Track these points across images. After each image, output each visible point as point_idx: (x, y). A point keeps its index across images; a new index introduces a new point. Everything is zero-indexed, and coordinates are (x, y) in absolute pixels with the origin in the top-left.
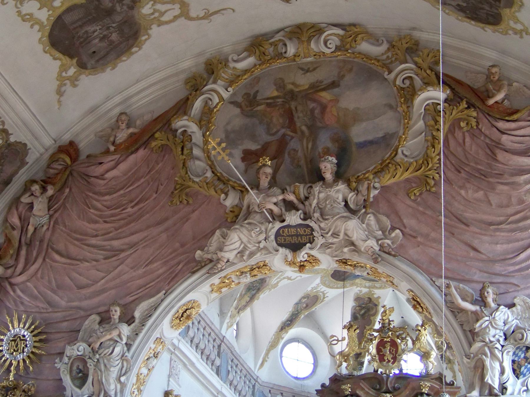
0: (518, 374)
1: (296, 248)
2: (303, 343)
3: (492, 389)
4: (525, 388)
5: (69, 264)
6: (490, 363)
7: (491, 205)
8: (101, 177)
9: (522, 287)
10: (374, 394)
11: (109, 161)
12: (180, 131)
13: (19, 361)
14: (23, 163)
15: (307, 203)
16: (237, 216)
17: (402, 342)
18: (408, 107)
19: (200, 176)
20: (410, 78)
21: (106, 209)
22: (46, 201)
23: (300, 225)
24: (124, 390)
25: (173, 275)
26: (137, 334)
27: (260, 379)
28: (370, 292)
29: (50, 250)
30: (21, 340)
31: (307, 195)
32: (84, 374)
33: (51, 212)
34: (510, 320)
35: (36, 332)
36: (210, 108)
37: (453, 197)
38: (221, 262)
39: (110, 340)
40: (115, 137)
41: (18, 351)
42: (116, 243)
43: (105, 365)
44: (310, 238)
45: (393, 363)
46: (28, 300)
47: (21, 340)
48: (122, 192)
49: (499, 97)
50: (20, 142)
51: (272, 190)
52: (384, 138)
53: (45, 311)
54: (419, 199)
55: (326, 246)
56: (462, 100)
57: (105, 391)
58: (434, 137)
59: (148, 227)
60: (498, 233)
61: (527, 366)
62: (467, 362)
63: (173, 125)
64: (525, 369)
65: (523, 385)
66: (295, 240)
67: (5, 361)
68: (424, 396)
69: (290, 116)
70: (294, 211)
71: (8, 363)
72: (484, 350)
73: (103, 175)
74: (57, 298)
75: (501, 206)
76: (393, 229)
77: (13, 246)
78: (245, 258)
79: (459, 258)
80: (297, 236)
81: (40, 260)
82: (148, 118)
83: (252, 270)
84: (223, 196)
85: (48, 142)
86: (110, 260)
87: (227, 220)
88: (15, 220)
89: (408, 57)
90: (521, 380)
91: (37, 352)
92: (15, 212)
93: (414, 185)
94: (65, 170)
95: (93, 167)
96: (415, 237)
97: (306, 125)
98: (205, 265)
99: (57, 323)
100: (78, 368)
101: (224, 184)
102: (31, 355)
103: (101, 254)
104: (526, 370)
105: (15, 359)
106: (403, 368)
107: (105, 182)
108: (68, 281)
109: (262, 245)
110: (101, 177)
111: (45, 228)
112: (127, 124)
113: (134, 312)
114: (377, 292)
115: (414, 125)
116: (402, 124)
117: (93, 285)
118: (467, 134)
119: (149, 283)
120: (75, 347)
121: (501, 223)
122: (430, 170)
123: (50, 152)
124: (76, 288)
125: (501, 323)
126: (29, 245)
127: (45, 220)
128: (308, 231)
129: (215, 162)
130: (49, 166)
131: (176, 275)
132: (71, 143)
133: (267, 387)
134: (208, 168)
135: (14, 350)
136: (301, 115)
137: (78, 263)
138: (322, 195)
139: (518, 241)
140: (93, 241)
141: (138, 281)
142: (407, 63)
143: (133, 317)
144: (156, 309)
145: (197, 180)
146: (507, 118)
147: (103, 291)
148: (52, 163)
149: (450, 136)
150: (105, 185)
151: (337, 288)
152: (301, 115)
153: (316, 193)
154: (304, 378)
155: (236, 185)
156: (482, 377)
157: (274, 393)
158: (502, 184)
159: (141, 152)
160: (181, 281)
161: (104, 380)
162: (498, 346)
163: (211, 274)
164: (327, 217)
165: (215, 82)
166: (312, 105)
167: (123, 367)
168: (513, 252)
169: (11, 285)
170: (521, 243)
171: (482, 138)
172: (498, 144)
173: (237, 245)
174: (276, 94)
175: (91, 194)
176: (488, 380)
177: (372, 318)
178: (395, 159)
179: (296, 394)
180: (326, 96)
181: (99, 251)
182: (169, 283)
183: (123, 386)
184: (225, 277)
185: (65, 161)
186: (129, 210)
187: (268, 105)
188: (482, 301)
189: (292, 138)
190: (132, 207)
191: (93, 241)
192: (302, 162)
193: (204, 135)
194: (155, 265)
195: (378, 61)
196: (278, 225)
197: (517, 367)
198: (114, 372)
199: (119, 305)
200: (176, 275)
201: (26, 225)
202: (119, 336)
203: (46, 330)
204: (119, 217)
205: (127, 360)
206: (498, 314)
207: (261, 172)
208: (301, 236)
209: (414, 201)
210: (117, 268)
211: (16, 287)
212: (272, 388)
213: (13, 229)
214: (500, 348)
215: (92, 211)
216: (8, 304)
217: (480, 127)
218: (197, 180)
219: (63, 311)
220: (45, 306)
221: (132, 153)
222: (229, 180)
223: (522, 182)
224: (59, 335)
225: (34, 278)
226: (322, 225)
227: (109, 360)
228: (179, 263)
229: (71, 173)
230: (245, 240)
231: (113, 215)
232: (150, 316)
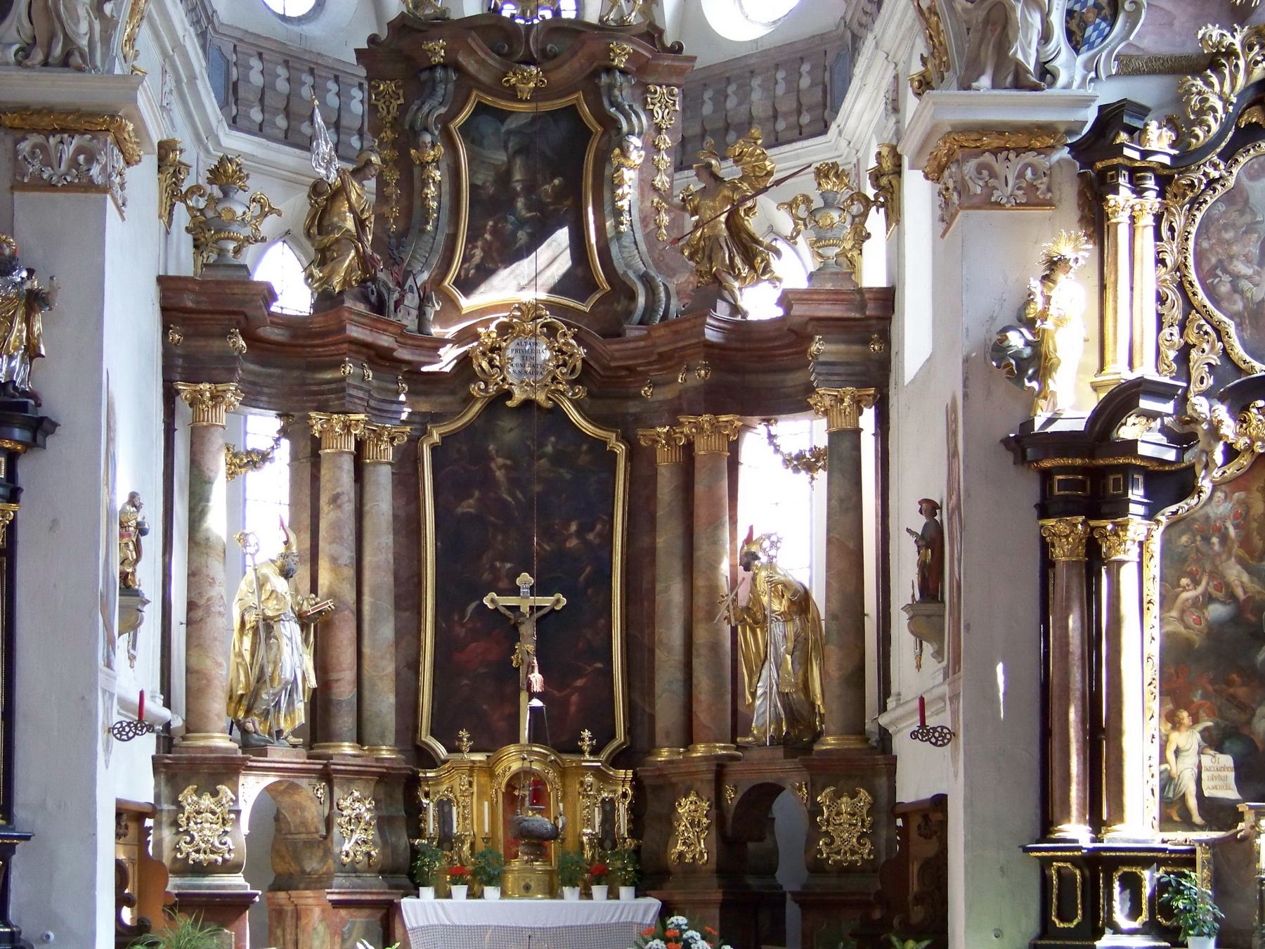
0: (1078, 43)
3: (1021, 71)
4: (1093, 74)
6: (1022, 11)
10: (497, 66)
24: (111, 36)
27: (218, 17)
57: (66, 35)
61: (1100, 24)
62: (965, 10)
64: (1094, 31)
65: (1087, 67)
68: (614, 74)
104: (1096, 33)
106: (562, 8)
133: (230, 37)
156: (1003, 45)
157: (242, 53)
176: (1016, 52)
179: (291, 56)
197: (1078, 25)
212: (241, 40)
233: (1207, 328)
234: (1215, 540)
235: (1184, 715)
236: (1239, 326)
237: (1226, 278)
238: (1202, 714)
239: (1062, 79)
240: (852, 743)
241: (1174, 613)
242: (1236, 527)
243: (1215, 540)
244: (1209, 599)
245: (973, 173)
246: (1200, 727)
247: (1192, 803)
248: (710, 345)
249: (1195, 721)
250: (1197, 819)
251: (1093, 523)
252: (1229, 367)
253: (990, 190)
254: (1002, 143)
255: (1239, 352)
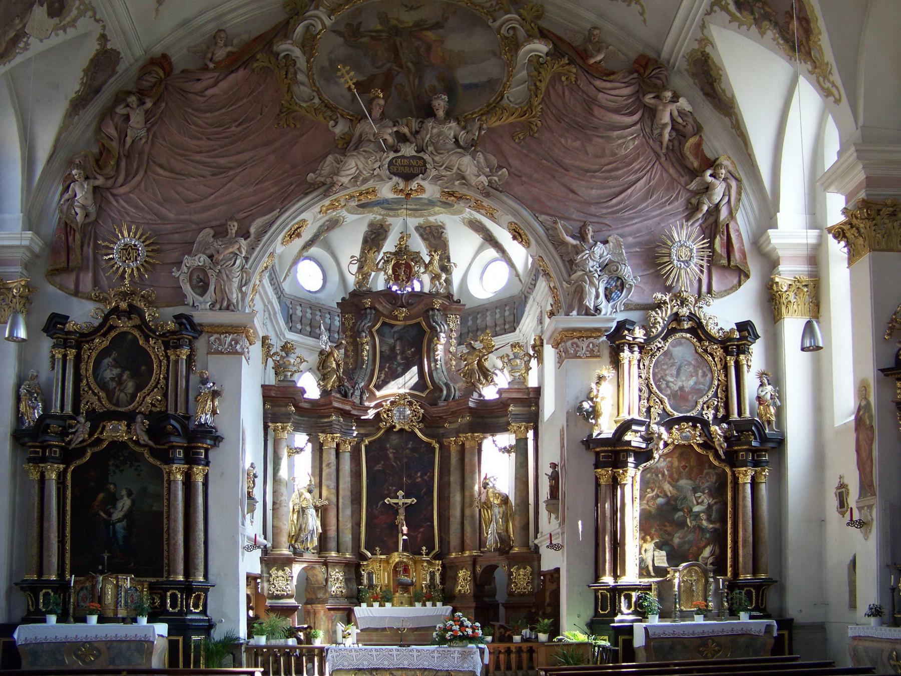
1: (408, 177)
5: (174, 178)
7: (588, 154)
8: (201, 93)
9: (613, 227)
11: (208, 79)
12: (283, 54)
13: (132, 269)
14: (114, 72)
15: (419, 136)
16: (348, 143)
17: (415, 264)
18: (512, 56)
19: (306, 102)
20: (514, 28)
22: (143, 114)
23: (413, 157)
25: (286, 195)
28: (383, 219)
29: (151, 163)
30: (132, 249)
31: (418, 129)
33: (148, 126)
34: (605, 254)
35: (147, 243)
36: (312, 34)
37: (555, 145)
38: (336, 186)
39: (231, 253)
40: (213, 54)
41: (130, 259)
43: (227, 276)
44: (421, 170)
45: (407, 282)
48: (224, 110)
49: (599, 58)
50: (115, 50)
51: (384, 121)
52: (488, 82)
54: (522, 143)
55: (438, 178)
56: (563, 56)
58: (537, 88)
60: (593, 180)
62: (567, 287)
63: (275, 47)
66: (407, 170)
67: (118, 268)
69: (395, 51)
70: (408, 144)
71: (121, 270)
72: (585, 279)
73: (202, 92)
74: (164, 211)
75: (596, 156)
76: (500, 167)
78: (358, 183)
79: (560, 199)
80: (410, 166)
82: (245, 37)
83: (361, 194)
84: (332, 123)
85: (138, 52)
87: (337, 145)
88: (111, 131)
89: (512, 8)
90: (611, 304)
93: (518, 129)
94: (160, 84)
95: (191, 83)
96: (519, 177)
97: (412, 62)
98: (319, 187)
100: (198, 277)
101: (332, 111)
102: (145, 264)
105: (128, 267)
107: (205, 99)
109: (375, 173)
110: (201, 93)
111: (144, 141)
112: (225, 43)
113: (250, 227)
114: (390, 220)
115: (518, 73)
116: (506, 71)
117: (201, 200)
118: (566, 88)
121: (595, 171)
122: (533, 117)
123: (140, 63)
125: (597, 256)
126: (128, 156)
127: (143, 133)
128: (421, 162)
129: (320, 89)
130: (140, 78)
131: (288, 195)
132: (165, 56)
134: (315, 94)
136: (406, 51)
138: (435, 131)
139: (610, 187)
140: (197, 157)
141: (250, 199)
142: (511, 13)
143: (248, 232)
144: (271, 226)
145: (304, 105)
146: (604, 78)
147: (213, 206)
148: (145, 74)
149: (550, 88)
150: (204, 102)
151: (357, 214)
152: (406, 51)
153: (430, 129)
154: (316, 292)
155: (344, 113)
156: (581, 299)
158: (598, 136)
159: (241, 73)
160: (294, 201)
162: (596, 275)
163: (326, 195)
164: (441, 152)
165: (317, 8)
166: (417, 43)
167: (242, 278)
168: (606, 197)
169: (114, 195)
170: (612, 190)
171: (580, 93)
172: (594, 101)
173: (353, 170)
174: (379, 27)
175: (190, 111)
177: (381, 242)
178: (501, 103)
180: (430, 35)
181: (205, 168)
182: (282, 203)
183: (244, 295)
184: (335, 200)
185: (158, 74)
186: (233, 129)
187: (372, 37)
188: (582, 237)
189: (398, 73)
190: (237, 126)
191: (197, 157)
192: (410, 97)
193: (308, 62)
194: (266, 184)
195: (483, 8)
196: (392, 155)
198: (236, 282)
200: (288, 195)
202: (239, 249)
204: (222, 135)
205: (246, 272)
206: (596, 248)
207: (375, 102)
208: (413, 167)
209: (518, 144)
210: (226, 184)
214: (597, 276)
215: (192, 127)
217: (578, 83)
218: (304, 105)
219: (173, 224)
220: (154, 217)
221: (232, 72)
222: (336, 108)
223: (615, 137)
224: (171, 246)
226: (437, 158)
227: (231, 271)
229: (166, 88)
230: (361, 166)
232: (266, 232)
233: (657, 400)
234: (660, 475)
235: (648, 537)
236: (669, 399)
237: (664, 382)
238: (655, 537)
239: (603, 312)
240: (524, 550)
241: (645, 502)
242: (668, 471)
243: (660, 475)
244: (658, 496)
245: (570, 346)
246: (654, 542)
247: (651, 568)
248: (470, 408)
249: (652, 539)
250: (653, 574)
251: (615, 470)
252: (665, 414)
253: (576, 352)
254: (581, 335)
255: (669, 408)
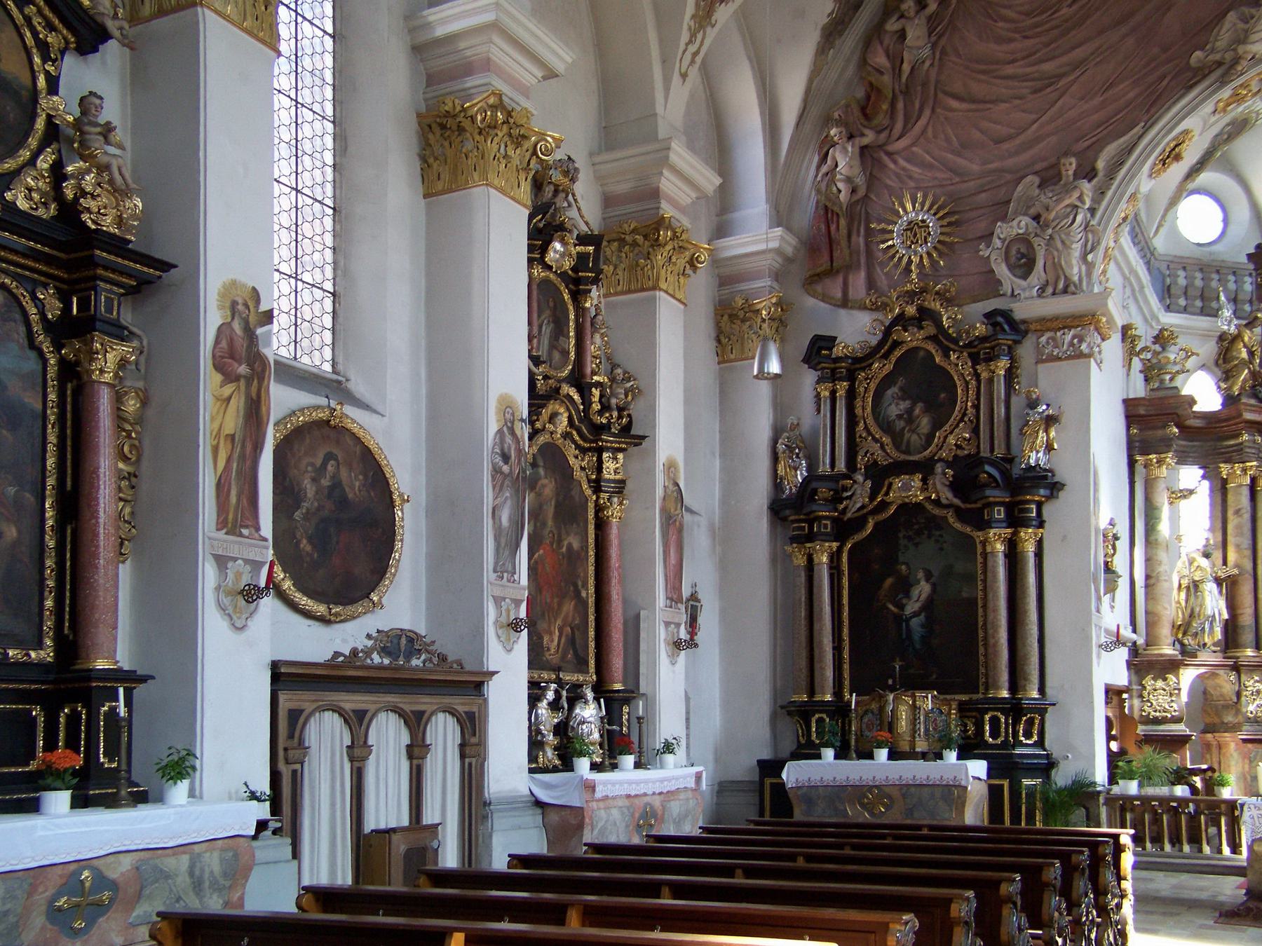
2: (1206, 195)
13: (921, 257)
21: (1024, 17)
26: (1103, 193)
32: (1028, 259)
41: (917, 242)
42: (1047, 67)
43: (1063, 242)
46: (920, 171)
47: (920, 227)
53: (949, 182)
57: (1066, 277)
59: (1101, 32)
67: (900, 259)
71: (905, 260)
74: (961, 161)
77: (886, 97)
81: (927, 112)
86: (1044, 93)
88: (881, 60)
91: (947, 239)
92: (879, 47)
98: (1210, 72)
99: (969, 196)
100: (1018, 251)
102: (939, 246)
103: (1027, 87)
108: (977, 135)
111: (927, 64)
113: (1095, 160)
119: (1113, 118)
120: (1015, 223)
124: (991, 143)
126: (907, 92)
127: (926, 52)
135: (912, 243)
137: (988, 106)
140: (1009, 70)
147: (1037, 140)
161: (1063, 263)
167: (1087, 241)
182: (1148, 111)
183: (1090, 266)
191: (1009, 70)
198: (1076, 249)
199: (1074, 155)
201: (898, 64)
203: (957, 209)
204: (1047, 26)
205: (1092, 232)
210: (1056, 102)
211: (896, 157)
212: (1172, 262)
213: (881, 73)
215: (1001, 24)
216: (889, 182)
220: (947, 175)
225: (922, 140)
227: (1068, 234)
228: (1162, 78)
231: (1036, 26)
